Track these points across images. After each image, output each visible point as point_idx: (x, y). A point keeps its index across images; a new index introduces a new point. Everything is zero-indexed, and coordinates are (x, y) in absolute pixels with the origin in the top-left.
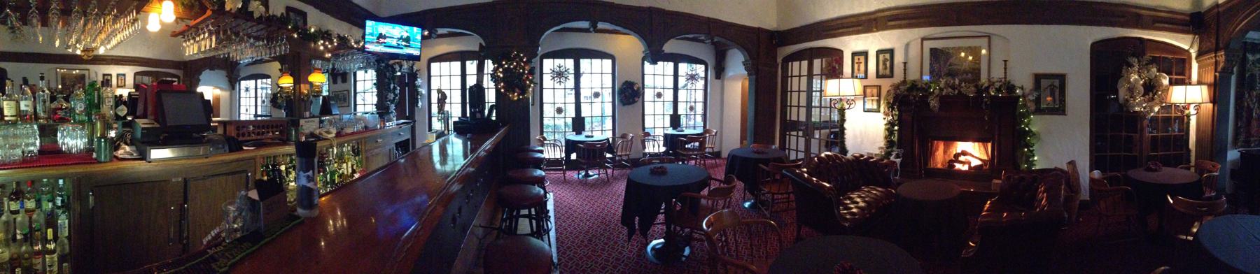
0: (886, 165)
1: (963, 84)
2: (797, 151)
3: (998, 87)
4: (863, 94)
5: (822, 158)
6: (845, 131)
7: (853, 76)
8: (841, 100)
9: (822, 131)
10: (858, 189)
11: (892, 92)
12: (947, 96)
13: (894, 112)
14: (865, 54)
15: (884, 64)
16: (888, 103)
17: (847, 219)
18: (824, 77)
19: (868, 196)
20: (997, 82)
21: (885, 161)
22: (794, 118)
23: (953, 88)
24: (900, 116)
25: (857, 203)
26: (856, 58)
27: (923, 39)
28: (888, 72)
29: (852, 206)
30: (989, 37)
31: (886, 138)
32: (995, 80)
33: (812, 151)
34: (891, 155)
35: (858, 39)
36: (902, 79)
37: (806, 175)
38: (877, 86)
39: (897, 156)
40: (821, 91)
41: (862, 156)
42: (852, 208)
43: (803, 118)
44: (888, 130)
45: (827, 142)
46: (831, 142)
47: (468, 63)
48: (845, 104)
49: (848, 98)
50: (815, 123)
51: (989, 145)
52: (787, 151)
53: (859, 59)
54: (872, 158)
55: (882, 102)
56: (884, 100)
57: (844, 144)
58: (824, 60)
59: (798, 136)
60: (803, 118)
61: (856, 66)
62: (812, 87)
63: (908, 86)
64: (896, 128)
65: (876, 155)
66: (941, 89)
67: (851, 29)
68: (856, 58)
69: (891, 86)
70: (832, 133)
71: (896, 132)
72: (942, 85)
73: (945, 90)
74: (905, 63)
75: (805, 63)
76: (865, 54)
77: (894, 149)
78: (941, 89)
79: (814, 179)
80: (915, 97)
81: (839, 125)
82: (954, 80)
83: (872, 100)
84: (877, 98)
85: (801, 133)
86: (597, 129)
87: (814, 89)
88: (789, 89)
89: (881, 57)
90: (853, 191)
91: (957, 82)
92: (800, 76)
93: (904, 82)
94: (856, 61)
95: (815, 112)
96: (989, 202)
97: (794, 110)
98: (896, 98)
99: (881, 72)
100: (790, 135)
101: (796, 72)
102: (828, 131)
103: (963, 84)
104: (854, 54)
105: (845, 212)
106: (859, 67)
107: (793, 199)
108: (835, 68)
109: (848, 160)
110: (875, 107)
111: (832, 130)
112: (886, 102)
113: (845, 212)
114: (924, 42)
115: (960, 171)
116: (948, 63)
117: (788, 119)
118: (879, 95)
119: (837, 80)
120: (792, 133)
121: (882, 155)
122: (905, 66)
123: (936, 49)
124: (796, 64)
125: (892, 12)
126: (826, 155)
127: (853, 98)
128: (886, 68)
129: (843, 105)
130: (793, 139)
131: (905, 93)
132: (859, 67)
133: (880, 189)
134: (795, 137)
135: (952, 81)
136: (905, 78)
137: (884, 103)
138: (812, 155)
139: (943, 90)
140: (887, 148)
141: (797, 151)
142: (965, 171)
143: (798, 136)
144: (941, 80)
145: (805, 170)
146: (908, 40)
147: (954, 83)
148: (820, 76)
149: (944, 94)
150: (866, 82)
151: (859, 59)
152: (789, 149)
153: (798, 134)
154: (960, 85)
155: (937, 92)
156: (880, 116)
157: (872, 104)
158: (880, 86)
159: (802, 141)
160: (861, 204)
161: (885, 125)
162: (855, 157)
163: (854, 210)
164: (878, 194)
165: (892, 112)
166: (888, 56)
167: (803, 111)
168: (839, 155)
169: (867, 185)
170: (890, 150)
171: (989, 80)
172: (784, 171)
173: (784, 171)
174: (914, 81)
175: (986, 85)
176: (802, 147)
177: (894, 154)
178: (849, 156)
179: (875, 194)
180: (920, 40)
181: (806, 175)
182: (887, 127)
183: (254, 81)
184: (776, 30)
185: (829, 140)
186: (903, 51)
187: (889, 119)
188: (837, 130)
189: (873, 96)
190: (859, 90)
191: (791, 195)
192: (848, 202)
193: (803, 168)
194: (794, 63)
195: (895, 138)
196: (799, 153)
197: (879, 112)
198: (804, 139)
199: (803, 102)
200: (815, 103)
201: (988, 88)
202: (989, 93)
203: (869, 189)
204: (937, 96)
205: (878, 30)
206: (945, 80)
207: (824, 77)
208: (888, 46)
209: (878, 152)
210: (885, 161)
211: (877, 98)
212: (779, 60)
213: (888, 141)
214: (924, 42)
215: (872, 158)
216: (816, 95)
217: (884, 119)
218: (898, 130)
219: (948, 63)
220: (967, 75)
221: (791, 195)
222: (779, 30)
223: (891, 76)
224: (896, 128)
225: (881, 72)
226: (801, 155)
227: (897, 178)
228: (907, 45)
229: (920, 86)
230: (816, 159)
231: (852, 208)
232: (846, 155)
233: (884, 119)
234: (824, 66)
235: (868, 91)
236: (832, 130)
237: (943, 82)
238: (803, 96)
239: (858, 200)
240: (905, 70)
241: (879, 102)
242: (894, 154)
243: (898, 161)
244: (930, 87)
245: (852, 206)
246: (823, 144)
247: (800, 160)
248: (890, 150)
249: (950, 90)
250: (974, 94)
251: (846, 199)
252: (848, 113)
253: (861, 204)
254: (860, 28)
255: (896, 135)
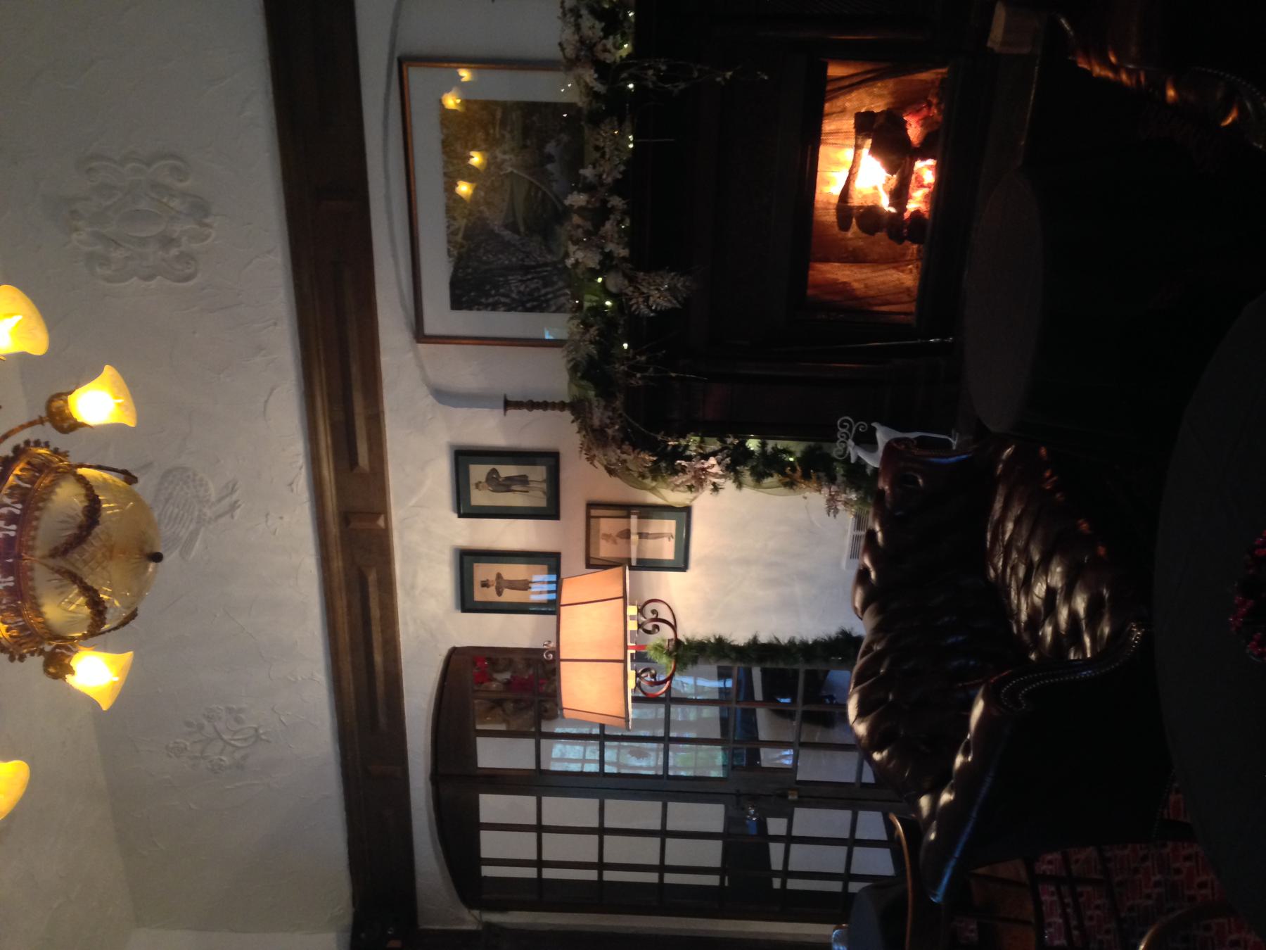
0: (901, 480)
1: (588, 172)
2: (852, 842)
3: (599, 25)
4: (618, 570)
5: (871, 731)
6: (763, 639)
7: (552, 608)
8: (640, 657)
9: (763, 735)
10: (998, 592)
11: (614, 454)
12: (632, 238)
13: (692, 450)
14: (467, 559)
15: (505, 485)
16: (655, 472)
17: (1115, 634)
18: (545, 727)
19: (1025, 552)
20: (578, 28)
21: (883, 485)
22: (711, 854)
23: (599, 214)
24: (707, 430)
25: (1051, 592)
26: (480, 595)
27: (420, 335)
28: (537, 473)
29: (1064, 614)
30: (403, 63)
31: (790, 484)
32: (569, 35)
33: (851, 778)
34: (860, 464)
35: (413, 587)
36: (567, 415)
37: (946, 797)
38: (589, 518)
39: (867, 441)
40: (602, 738)
41: (863, 575)
42: (1073, 615)
43: (711, 816)
44: (759, 477)
45: (809, 718)
46: (806, 701)
47: (555, 594)
48: (654, 640)
49: (632, 626)
50: (730, 767)
51: (835, 71)
52: (854, 887)
53: (485, 584)
54: (871, 535)
55: (652, 499)
56: (644, 488)
57: (816, 643)
58: (479, 727)
59: (789, 839)
60: (711, 816)
61: (510, 596)
62: (581, 774)
63: (592, 393)
64: (753, 444)
65: (859, 526)
66: (607, 264)
67: (375, 612)
68: (480, 595)
69: (591, 459)
70: (770, 697)
71: (771, 444)
72: (591, 259)
73: (610, 247)
74: (508, 404)
75: (492, 806)
76: (467, 559)
77: (835, 451)
78: (607, 264)
79: (959, 760)
80: (635, 368)
81: (737, 667)
82: (569, 211)
83: (642, 535)
84: (634, 520)
85: (776, 826)
86: (610, 755)
87: (593, 768)
88: (592, 875)
89: (480, 498)
90: (1008, 614)
91: (578, 199)
92: (539, 829)
93: (577, 408)
94: (489, 595)
95: (684, 762)
96: (664, 352)
97: (679, 852)
98: (640, 442)
99: (536, 499)
100: (786, 874)
101: (523, 846)
102: (762, 715)
103: (588, 172)
104: (467, 603)
105: (1087, 640)
106: (514, 585)
107: (1056, 856)
108: (508, 684)
109: (878, 630)
110: (669, 526)
111: (758, 695)
112: (649, 482)
113: (1087, 640)
114: (429, 329)
115: (939, 195)
116: (507, 234)
117: (713, 880)
118: (626, 509)
119: (566, 670)
120: (776, 863)
121: (862, 501)
122: (518, 405)
123: (455, 284)
124: (491, 844)
125: (323, 453)
126: (861, 714)
127: (632, 610)
128: (523, 480)
129: (658, 648)
130: (802, 858)
131: (618, 404)
132: (514, 585)
133: (998, 506)
134: (795, 848)
135: (576, 219)
136: (562, 406)
137: (653, 490)
138: (868, 777)
139: (608, 256)
140: (832, 480)
141: (852, 842)
142: (940, 171)
143: (789, 839)
144: (570, 262)
145: (924, 802)
146: (424, 390)
147: (581, 211)
148: (544, 742)
149: (624, 252)
150: (573, 560)
151: (485, 584)
152: (847, 877)
153: (777, 839)
154: (589, 188)
155: (615, 282)
156: (704, 505)
157: (659, 536)
158: (591, 505)
159: (808, 820)
160: (1056, 577)
161: (740, 485)
162: (865, 606)
163: (1080, 604)
164: (1016, 511)
165: (689, 459)
166: (478, 472)
167: (684, 815)
168: (860, 662)
169: (984, 558)
170: (840, 470)
171: (570, 64)
172: (938, 898)
173: (938, 898)
174: (574, 369)
175: (590, 76)
176: (833, 821)
177: (855, 452)
178: (861, 627)
179: (1017, 522)
180: (424, 348)
181: (946, 797)
182: (747, 477)
183: (562, 664)
184: (348, 936)
185: (800, 708)
186: (460, 413)
187: (716, 469)
188: (756, 673)
189: (626, 534)
190: (606, 583)
191: (1043, 867)
192: (1048, 630)
193: (917, 809)
194: (486, 852)
195: (795, 448)
196: (859, 835)
197: (687, 510)
198: (800, 813)
199: (645, 813)
200: (646, 762)
201: (605, 70)
202: (625, 64)
203: (999, 549)
204: (632, 280)
205: (382, 509)
206: (572, 248)
207: (545, 727)
208: (442, 469)
209: (847, 519)
210: (883, 485)
211: (634, 520)
212: (470, 920)
213: (806, 476)
214: (429, 329)
215: (871, 535)
216: (620, 759)
217: (716, 488)
218: (763, 436)
219: (507, 234)
220: (550, 158)
221: (1043, 867)
222: (348, 920)
223: (551, 460)
224: (753, 444)
225: (536, 499)
226: (871, 824)
227: (954, 443)
228: (444, 396)
229: (592, 350)
230: (877, 756)
231: (1073, 615)
232: (859, 640)
233: (716, 488)
234: (503, 727)
235: (605, 550)
236: (758, 695)
237: (580, 256)
238: (621, 812)
239: (1040, 589)
240: (532, 405)
241: (649, 511)
242: (855, 452)
243: (883, 436)
244: (598, 310)
245: (1064, 614)
246: (819, 735)
247: (890, 827)
248: (840, 470)
249: (608, 226)
250: (628, 125)
251: (1038, 641)
252: (694, 628)
253: (1056, 577)
254: (372, 577)
255: (781, 444)
